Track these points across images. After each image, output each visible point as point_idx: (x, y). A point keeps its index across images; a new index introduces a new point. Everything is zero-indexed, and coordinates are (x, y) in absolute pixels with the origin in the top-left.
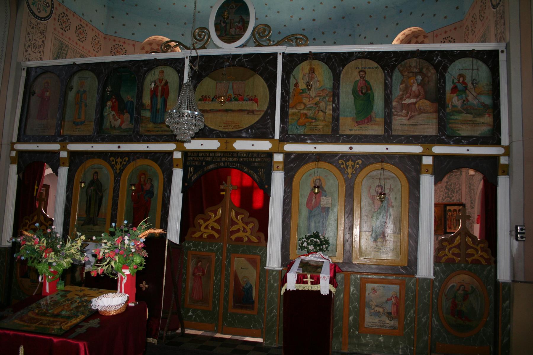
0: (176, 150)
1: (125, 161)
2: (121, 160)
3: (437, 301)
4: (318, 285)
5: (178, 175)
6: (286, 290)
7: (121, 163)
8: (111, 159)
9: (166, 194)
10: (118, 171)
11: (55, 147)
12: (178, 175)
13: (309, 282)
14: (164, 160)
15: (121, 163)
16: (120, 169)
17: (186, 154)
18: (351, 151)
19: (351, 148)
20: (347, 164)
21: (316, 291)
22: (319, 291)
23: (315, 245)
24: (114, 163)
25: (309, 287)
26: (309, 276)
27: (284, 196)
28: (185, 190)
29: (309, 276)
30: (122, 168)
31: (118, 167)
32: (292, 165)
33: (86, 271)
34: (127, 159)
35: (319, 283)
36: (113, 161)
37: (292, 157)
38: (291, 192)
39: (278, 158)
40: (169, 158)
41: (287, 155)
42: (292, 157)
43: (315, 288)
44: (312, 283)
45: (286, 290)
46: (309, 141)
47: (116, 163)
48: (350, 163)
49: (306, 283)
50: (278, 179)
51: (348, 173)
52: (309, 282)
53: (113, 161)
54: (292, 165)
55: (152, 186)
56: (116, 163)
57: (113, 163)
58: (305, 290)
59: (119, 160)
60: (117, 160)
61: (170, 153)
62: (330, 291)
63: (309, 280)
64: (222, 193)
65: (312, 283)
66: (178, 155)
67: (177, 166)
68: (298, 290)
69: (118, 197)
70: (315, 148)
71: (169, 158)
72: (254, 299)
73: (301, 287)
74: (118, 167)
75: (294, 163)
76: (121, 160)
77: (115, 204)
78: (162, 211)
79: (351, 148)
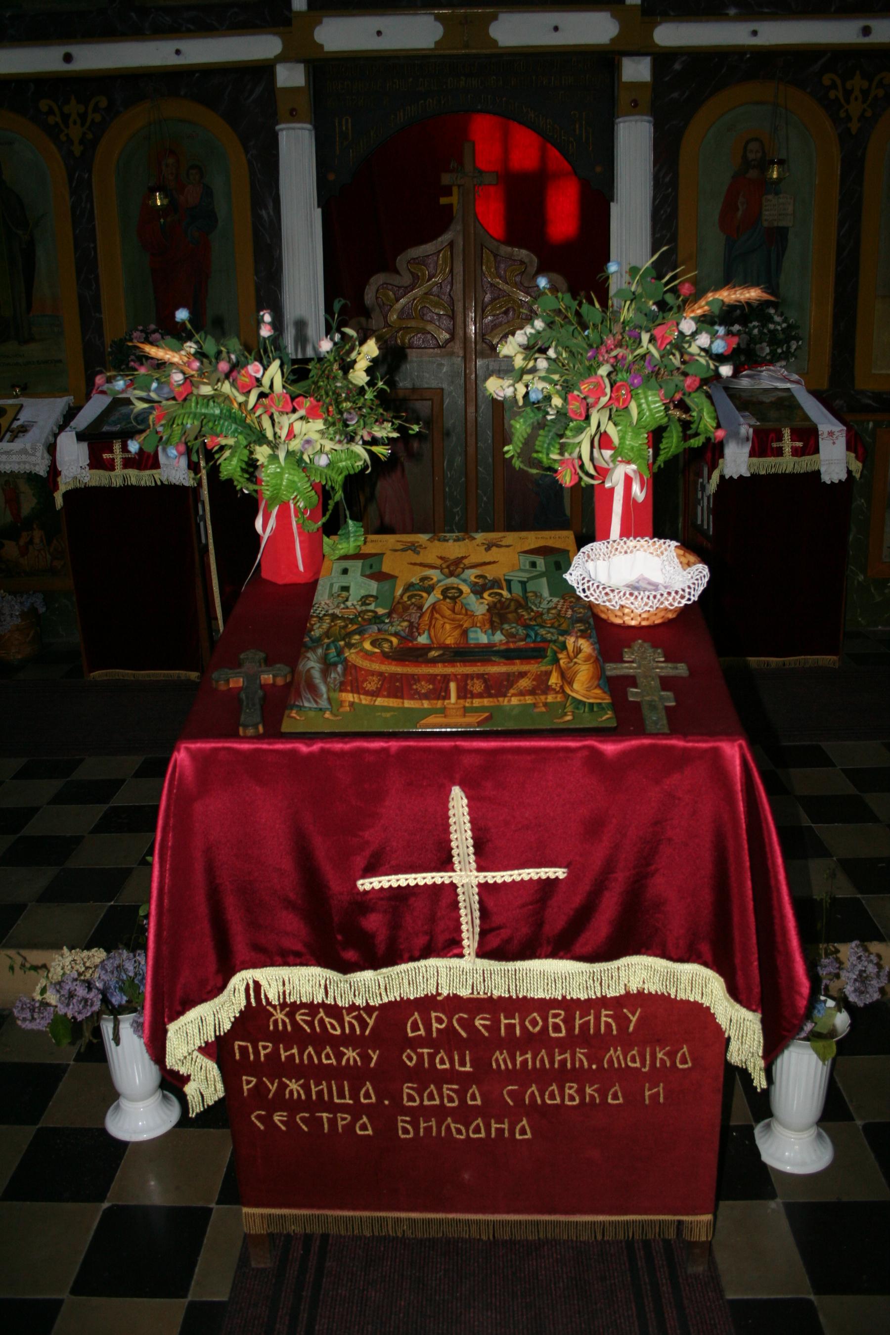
0: (282, 58)
1: (96, 109)
2: (82, 109)
3: (477, 469)
4: (815, 457)
5: (297, 151)
6: (722, 477)
7: (865, 93)
8: (44, 105)
9: (264, 213)
10: (77, 150)
11: (261, 47)
12: (297, 151)
13: (787, 450)
14: (243, 96)
15: (83, 117)
16: (81, 142)
17: (326, 69)
18: (866, 40)
19: (866, 31)
20: (849, 85)
21: (806, 474)
22: (818, 473)
23: (774, 341)
24: (58, 119)
25: (787, 463)
26: (787, 433)
27: (654, 199)
28: (330, 199)
29: (787, 433)
30: (90, 136)
31: (75, 132)
32: (675, 95)
33: (63, 488)
34: (104, 103)
35: (817, 451)
36: (51, 112)
37: (677, 66)
38: (674, 184)
39: (636, 70)
40: (258, 90)
41: (663, 59)
42: (677, 66)
43: (804, 464)
44: (796, 452)
45: (722, 477)
46: (732, 12)
47: (848, 93)
48: (857, 83)
49: (779, 452)
50: (634, 143)
51: (849, 118)
52: (787, 450)
53: (51, 112)
54: (675, 95)
55: (208, 192)
56: (848, 93)
57: (51, 120)
58: (776, 475)
59: (73, 108)
60: (66, 110)
61: (264, 71)
62: (849, 472)
63: (787, 444)
64: (443, 201)
65: (796, 452)
66: (291, 76)
67: (293, 115)
68: (754, 476)
69: (94, 241)
70: (178, 52)
71: (258, 90)
72: (568, 512)
73: (766, 465)
74: (75, 132)
75: (686, 84)
76: (82, 109)
77: (86, 266)
78: (256, 273)
79: (68, 58)
